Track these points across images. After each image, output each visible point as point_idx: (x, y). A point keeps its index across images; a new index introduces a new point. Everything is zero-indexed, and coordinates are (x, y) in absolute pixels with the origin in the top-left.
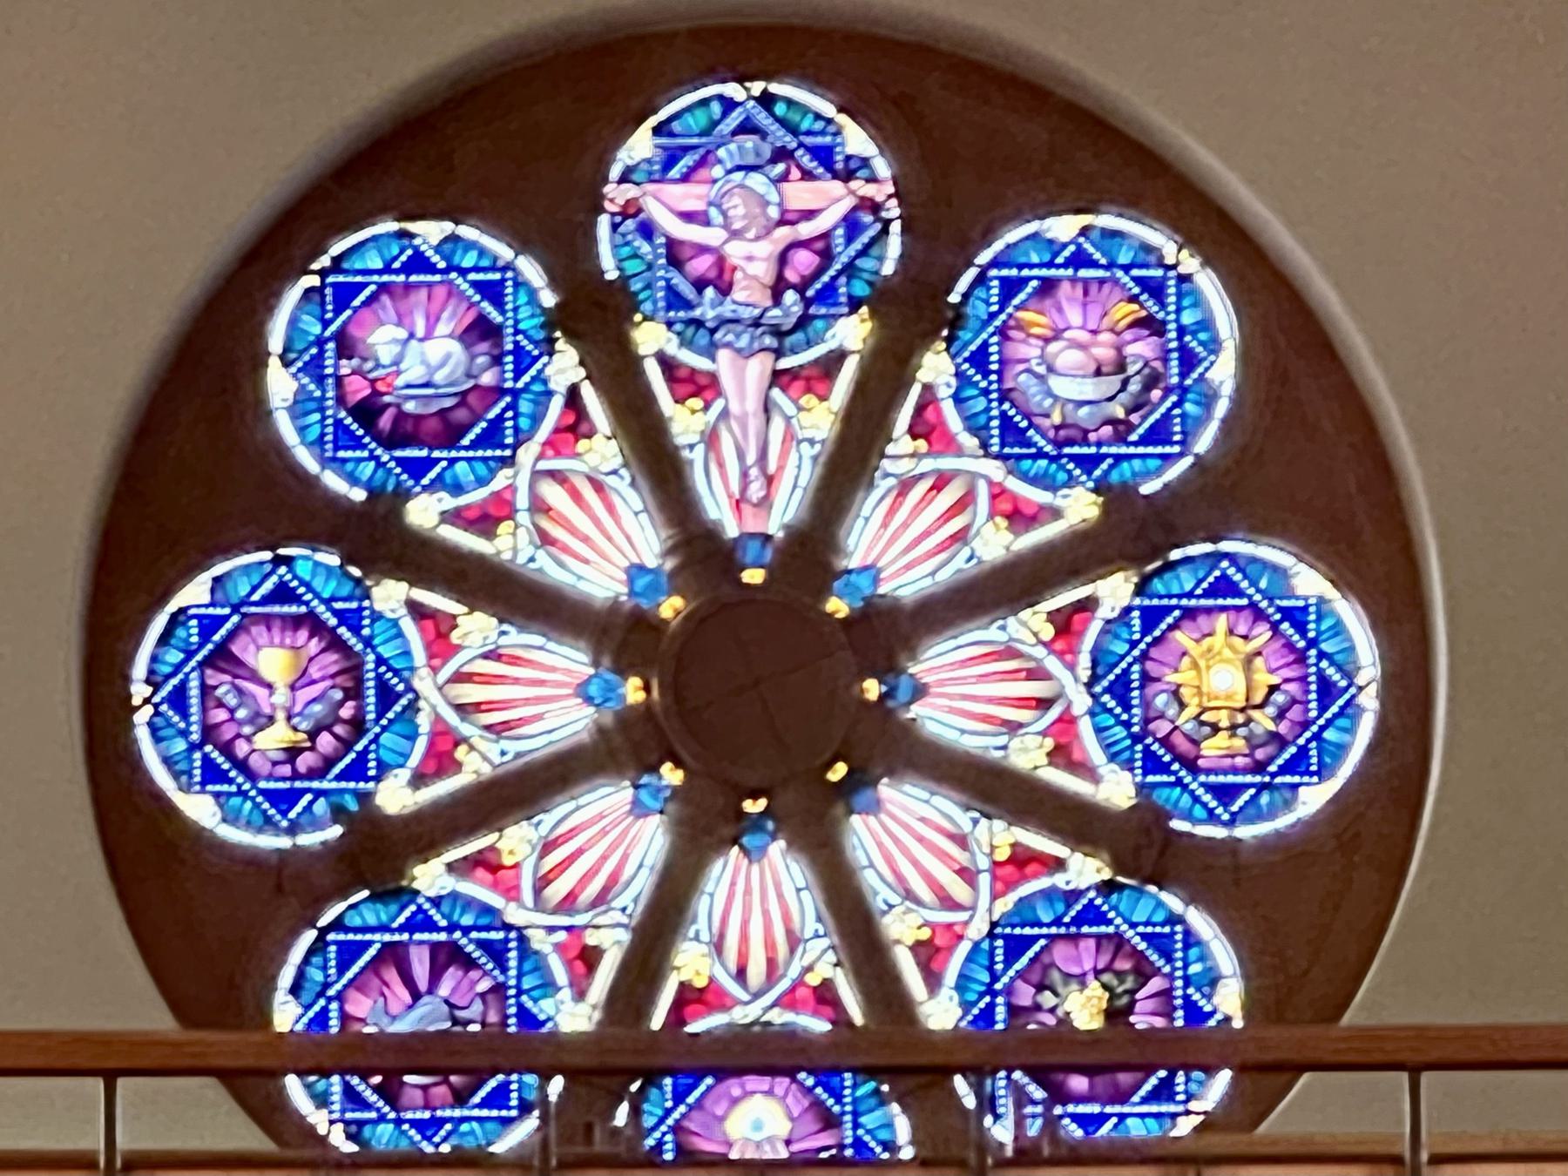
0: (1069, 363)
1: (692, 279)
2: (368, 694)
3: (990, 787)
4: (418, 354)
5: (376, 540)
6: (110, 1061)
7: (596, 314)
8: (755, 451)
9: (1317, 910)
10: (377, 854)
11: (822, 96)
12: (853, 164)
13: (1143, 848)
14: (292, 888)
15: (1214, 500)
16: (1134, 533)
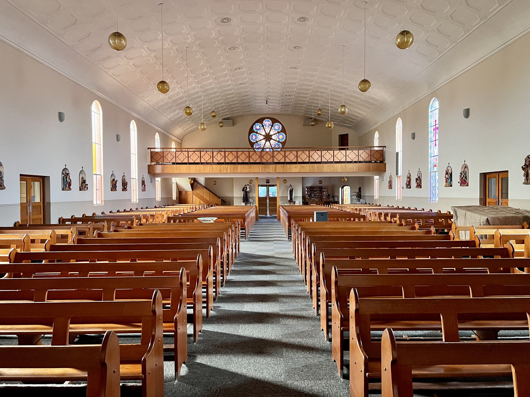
0: (276, 128)
1: (266, 125)
2: (256, 138)
3: (275, 140)
4: (258, 127)
5: (257, 133)
6: (249, 148)
7: (263, 126)
8: (268, 130)
9: (283, 143)
10: (257, 142)
11: (468, 370)
12: (64, 172)
13: (279, 142)
14: (255, 143)
15: (281, 132)
16: (278, 132)
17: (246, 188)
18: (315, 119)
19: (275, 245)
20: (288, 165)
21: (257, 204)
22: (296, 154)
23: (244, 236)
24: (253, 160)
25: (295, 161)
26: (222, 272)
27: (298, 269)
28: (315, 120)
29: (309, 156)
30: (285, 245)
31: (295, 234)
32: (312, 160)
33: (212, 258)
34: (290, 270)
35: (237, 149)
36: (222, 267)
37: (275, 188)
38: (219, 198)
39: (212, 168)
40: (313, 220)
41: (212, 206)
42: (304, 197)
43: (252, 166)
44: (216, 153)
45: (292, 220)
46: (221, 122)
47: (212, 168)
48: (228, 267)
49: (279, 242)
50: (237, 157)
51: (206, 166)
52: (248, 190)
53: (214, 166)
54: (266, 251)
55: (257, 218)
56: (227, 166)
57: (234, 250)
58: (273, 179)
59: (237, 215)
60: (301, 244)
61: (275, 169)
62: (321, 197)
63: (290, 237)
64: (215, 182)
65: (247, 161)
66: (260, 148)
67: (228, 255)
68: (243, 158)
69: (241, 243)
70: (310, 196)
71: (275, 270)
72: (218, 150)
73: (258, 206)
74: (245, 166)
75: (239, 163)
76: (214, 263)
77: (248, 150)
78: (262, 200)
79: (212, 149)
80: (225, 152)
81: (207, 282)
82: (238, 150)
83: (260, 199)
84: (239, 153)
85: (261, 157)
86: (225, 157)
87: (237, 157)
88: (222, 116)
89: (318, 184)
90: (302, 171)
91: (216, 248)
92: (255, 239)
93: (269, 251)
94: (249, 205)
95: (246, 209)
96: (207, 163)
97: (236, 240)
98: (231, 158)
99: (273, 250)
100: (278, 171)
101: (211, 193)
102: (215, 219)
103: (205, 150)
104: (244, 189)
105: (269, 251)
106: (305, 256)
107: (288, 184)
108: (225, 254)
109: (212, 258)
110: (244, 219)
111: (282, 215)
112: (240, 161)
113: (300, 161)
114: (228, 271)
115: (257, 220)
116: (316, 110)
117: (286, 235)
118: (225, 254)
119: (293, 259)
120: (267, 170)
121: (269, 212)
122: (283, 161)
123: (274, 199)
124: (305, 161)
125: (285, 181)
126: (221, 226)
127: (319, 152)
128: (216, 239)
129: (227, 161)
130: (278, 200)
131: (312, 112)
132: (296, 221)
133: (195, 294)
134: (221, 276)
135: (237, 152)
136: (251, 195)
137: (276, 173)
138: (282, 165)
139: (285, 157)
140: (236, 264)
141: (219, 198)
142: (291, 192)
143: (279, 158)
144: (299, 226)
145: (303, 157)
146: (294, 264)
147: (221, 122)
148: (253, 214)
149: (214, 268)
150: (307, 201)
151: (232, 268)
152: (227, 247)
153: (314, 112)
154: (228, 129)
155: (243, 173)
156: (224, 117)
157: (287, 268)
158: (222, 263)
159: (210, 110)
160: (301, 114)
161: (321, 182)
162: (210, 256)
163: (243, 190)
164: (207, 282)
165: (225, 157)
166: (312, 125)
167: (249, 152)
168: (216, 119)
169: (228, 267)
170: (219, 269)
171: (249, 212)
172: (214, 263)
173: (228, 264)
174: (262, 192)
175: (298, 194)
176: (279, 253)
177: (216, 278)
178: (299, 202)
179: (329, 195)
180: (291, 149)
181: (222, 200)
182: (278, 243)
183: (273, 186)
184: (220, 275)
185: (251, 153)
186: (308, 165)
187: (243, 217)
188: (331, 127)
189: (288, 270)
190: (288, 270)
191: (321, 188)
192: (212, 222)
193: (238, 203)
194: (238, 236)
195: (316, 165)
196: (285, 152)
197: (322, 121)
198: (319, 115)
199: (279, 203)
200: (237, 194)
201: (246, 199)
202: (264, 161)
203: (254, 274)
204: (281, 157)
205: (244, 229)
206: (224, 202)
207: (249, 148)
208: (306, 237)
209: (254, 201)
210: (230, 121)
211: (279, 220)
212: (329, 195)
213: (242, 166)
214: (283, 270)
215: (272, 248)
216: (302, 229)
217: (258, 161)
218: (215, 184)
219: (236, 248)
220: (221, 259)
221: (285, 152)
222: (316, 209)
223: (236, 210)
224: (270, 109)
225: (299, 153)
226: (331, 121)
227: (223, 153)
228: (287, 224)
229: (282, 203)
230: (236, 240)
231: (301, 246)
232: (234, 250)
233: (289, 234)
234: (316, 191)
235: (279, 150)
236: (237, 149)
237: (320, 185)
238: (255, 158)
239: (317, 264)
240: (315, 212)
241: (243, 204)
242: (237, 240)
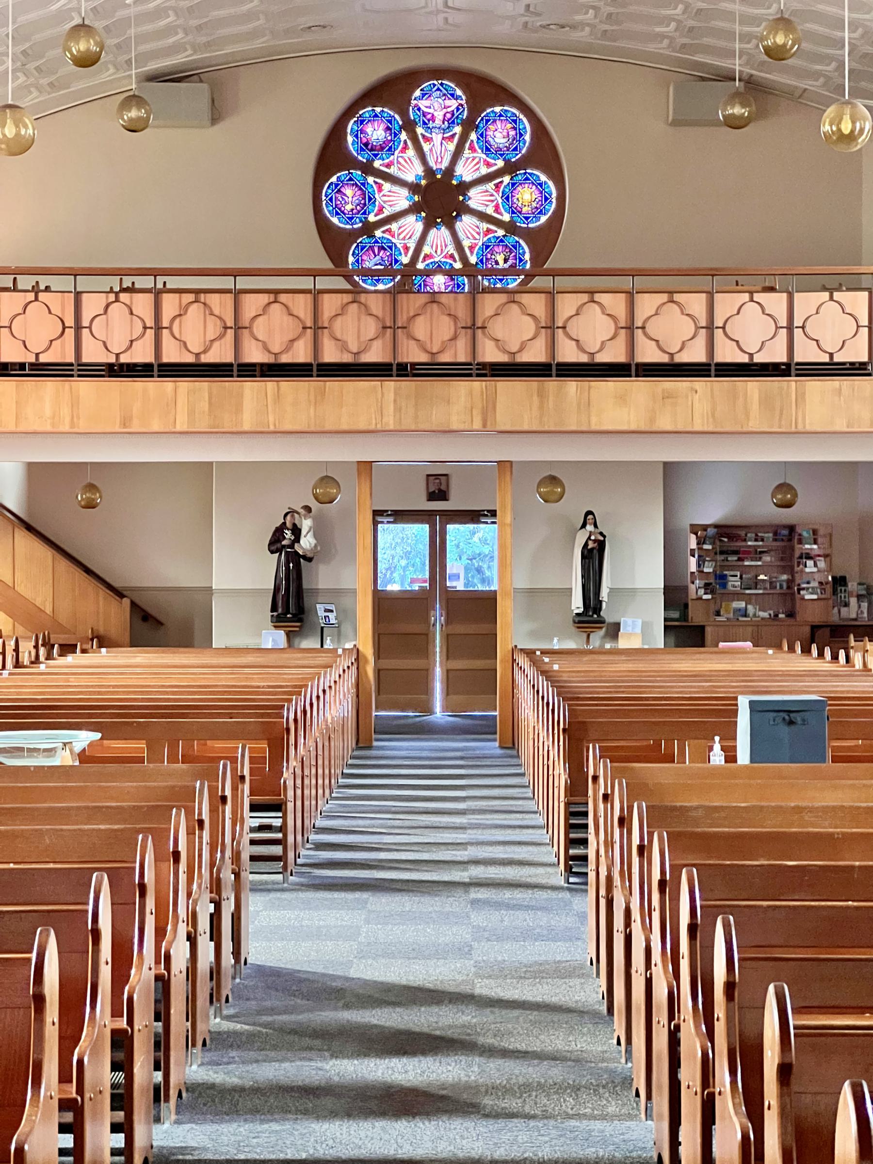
0: (499, 136)
2: (367, 200)
3: (483, 216)
4: (376, 133)
5: (368, 169)
6: (314, 273)
8: (439, 152)
14: (353, 235)
17: (297, 532)
18: (750, 82)
19: (479, 918)
20: (572, 386)
21: (362, 636)
22: (621, 311)
23: (273, 852)
24: (344, 347)
25: (615, 354)
26: (122, 1099)
27: (627, 1081)
28: (754, 90)
29: (710, 328)
30: (543, 919)
31: (609, 844)
32: (727, 354)
33: (52, 1013)
34: (576, 1089)
35: (235, 273)
36: (122, 1063)
37: (486, 531)
38: (119, 593)
39: (75, 403)
40: (731, 758)
41: (68, 649)
42: (674, 596)
43: (333, 385)
44: (102, 300)
45: (592, 752)
46: (133, 100)
47: (75, 403)
48: (161, 1063)
49: (507, 895)
50: (238, 328)
51: (30, 384)
52: (307, 542)
53: (85, 387)
54: (417, 953)
55: (364, 735)
56: (168, 385)
57: (206, 948)
58: (474, 471)
59: (231, 711)
60: (646, 912)
61: (489, 408)
62: (789, 597)
63: (575, 863)
64: (91, 487)
65: (301, 354)
66: (388, 272)
67: (163, 983)
68: (274, 334)
69: (254, 904)
70: (716, 584)
71: (474, 1088)
72: (114, 282)
73: (368, 651)
74: (288, 386)
75: (249, 371)
76: (69, 1038)
77: (306, 283)
78: (397, 617)
79: (75, 274)
80: (158, 294)
81: (80, 1090)
82: (243, 283)
83: (386, 607)
84: (252, 304)
85: (393, 328)
86: (158, 328)
87: (238, 328)
88: (142, 58)
89: (765, 510)
90: (665, 423)
91: (79, 938)
92: (350, 875)
93: (440, 953)
94: (310, 643)
95: (291, 676)
96: (39, 370)
97: (216, 886)
98: (195, 334)
99: (464, 951)
100: (503, 421)
101: (63, 564)
102: (83, 738)
103: (25, 282)
104: (279, 533)
105: (440, 953)
106: (673, 1000)
107: (573, 506)
108: (142, 977)
109: (52, 1013)
110: (279, 744)
111: (529, 713)
112: (254, 355)
113: (649, 354)
114: (159, 1094)
115: (362, 742)
116: (756, 20)
117: (552, 851)
118: (142, 977)
119: (594, 1015)
120: (436, 417)
121: (448, 691)
122: (535, 354)
123: (480, 608)
124: (685, 357)
125: (552, 484)
126: (124, 789)
127: (776, 303)
128: (82, 881)
129: (172, 355)
130: (505, 610)
131: (730, 35)
132: (614, 756)
133: (20, 1151)
134: (115, 1128)
135: (238, 294)
136: (320, 578)
137: (490, 431)
138: (530, 385)
139: (551, 328)
140: (219, 1042)
141: (119, 593)
142: (593, 557)
143: (514, 332)
144: (635, 792)
145: (672, 330)
146: (600, 1044)
147: (133, 100)
148: (338, 708)
149: (64, 1078)
150: (696, 616)
151: (191, 1069)
152: (160, 933)
153: (746, 38)
154: (180, 145)
155: (277, 434)
156: (154, 66)
157: (556, 1073)
158: (122, 1042)
159: (62, 15)
160: (661, 47)
161: (785, 493)
162: (39, 1000)
163: (275, 543)
164: (80, 1090)
165: (158, 328)
166: (735, 124)
167: (317, 294)
168: (105, 75)
169: (161, 1063)
170: (101, 1075)
171: (311, 691)
172: (69, 1038)
173: (162, 1044)
174: (400, 556)
175: (639, 572)
176: (501, 972)
177: (79, 1141)
178: (642, 624)
179: (840, 581)
180: (595, 277)
181: (133, 604)
182: (499, 905)
183: (473, 516)
184: (108, 1117)
185: (330, 304)
186: (700, 384)
187: (271, 727)
188: (851, 137)
189: (560, 1088)
190: (560, 1088)
191: (787, 535)
192: (64, 759)
193: (243, 628)
194: (236, 857)
195: (753, 386)
196: (551, 295)
197: (796, 98)
198: (776, 54)
199: (513, 631)
200: (240, 572)
201: (291, 605)
202: (413, 355)
203: (333, 1115)
204: (528, 327)
205: (278, 807)
206: (151, 622)
207: (314, 273)
208: (676, 870)
209: (347, 615)
210: (196, 95)
211: (511, 743)
212: (840, 581)
213: (270, 385)
214: (526, 1088)
215: (459, 933)
216: (658, 816)
217: (372, 356)
218: (91, 505)
219: (215, 935)
220: (116, 1013)
221: (551, 295)
222: (758, 671)
223: (225, 680)
224: (455, 18)
225: (647, 304)
226: (856, 93)
227: (143, 304)
228: (561, 775)
229: (534, 634)
230: (216, 886)
231: (648, 930)
232: (206, 948)
233: (571, 843)
234: (757, 554)
235: (513, 283)
236: (235, 273)
237: (786, 516)
238: (355, 333)
239: (746, 1056)
240: (743, 702)
241: (275, 638)
242: (228, 877)
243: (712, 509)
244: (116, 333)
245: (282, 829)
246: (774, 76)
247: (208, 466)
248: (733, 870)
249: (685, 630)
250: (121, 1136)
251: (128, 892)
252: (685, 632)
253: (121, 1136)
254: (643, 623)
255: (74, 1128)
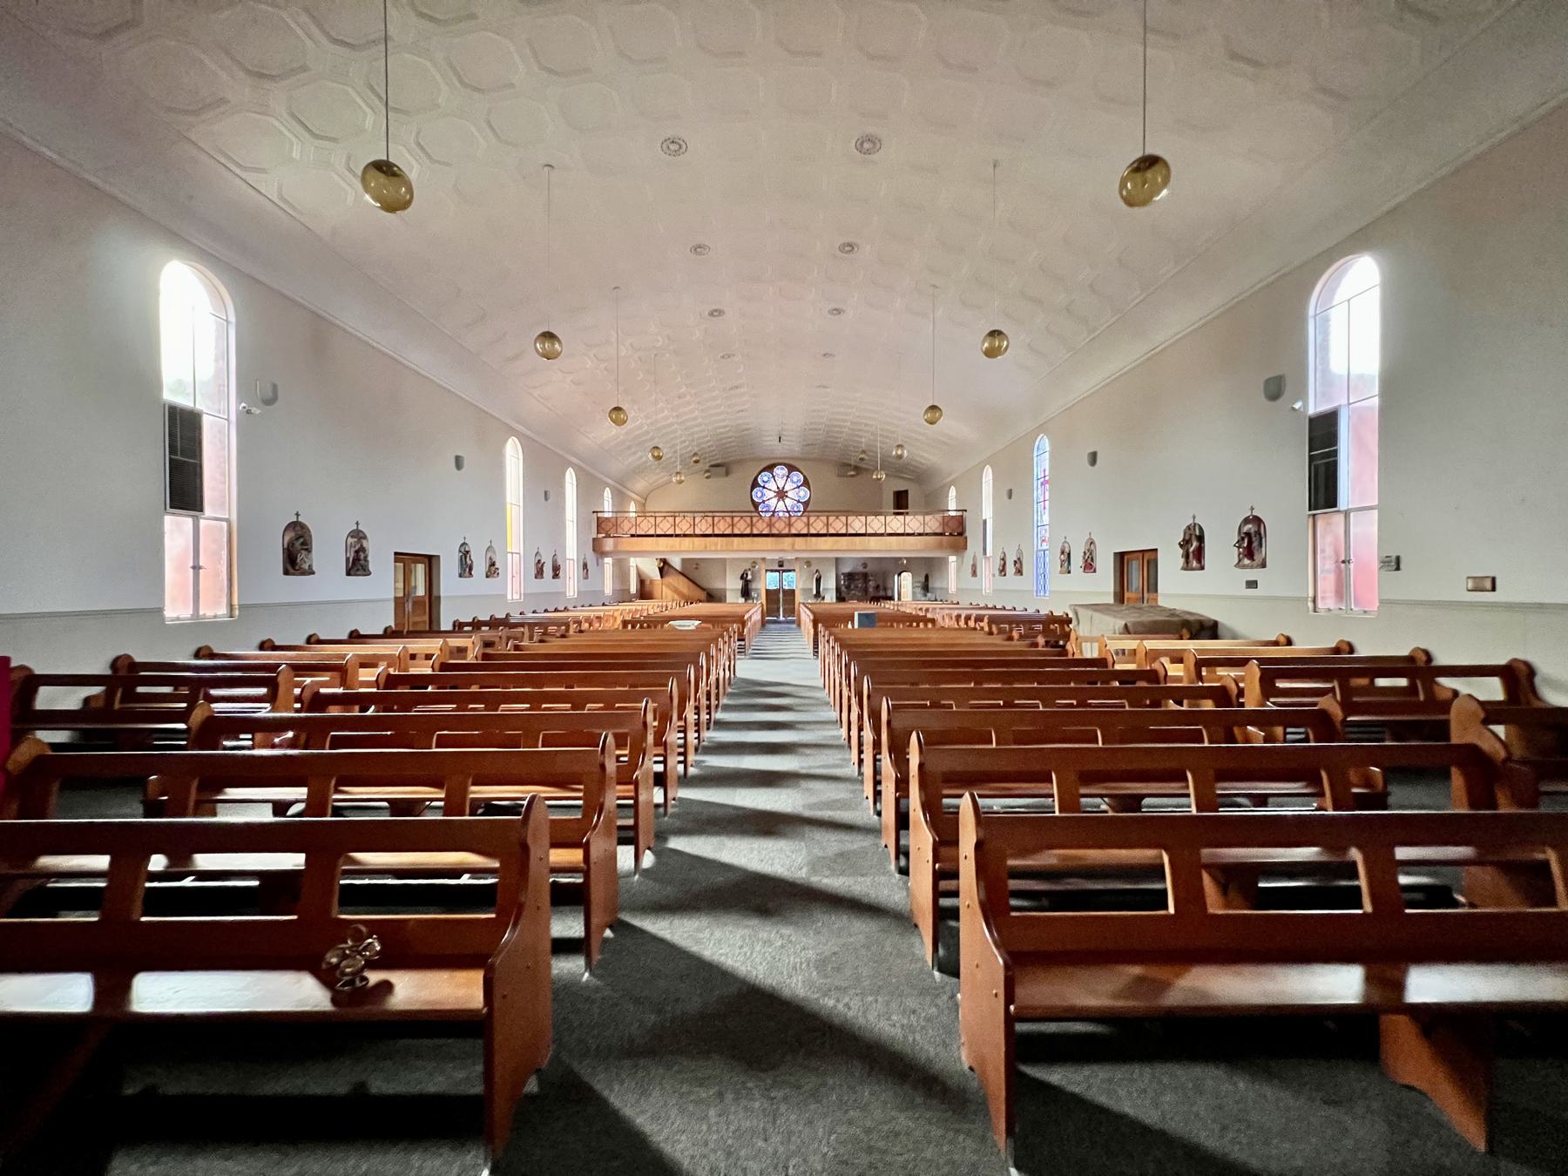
8: (781, 483)
26: (709, 707)
28: (856, 468)
32: (851, 531)
36: (709, 699)
55: (764, 623)
62: (866, 590)
63: (816, 653)
85: (770, 525)
89: (861, 569)
91: (698, 669)
92: (760, 656)
98: (722, 527)
107: (814, 568)
108: (713, 678)
110: (744, 624)
118: (713, 678)
125: (808, 563)
132: (826, 628)
136: (753, 586)
139: (808, 525)
142: (818, 581)
146: (823, 695)
148: (757, 617)
151: (724, 701)
155: (742, 550)
161: (865, 565)
168: (699, 466)
170: (704, 702)
172: (696, 691)
174: (770, 581)
175: (829, 584)
178: (830, 597)
191: (865, 576)
193: (734, 599)
199: (799, 598)
200: (733, 584)
201: (746, 593)
206: (712, 596)
210: (722, 470)
216: (836, 640)
239: (860, 695)
243: (847, 569)
244: (703, 527)
245: (635, 828)
246: (862, 465)
247: (724, 560)
248: (855, 652)
249: (840, 598)
250: (450, 628)
251: (709, 657)
252: (840, 599)
253: (450, 628)
254: (555, 845)
255: (698, 714)
